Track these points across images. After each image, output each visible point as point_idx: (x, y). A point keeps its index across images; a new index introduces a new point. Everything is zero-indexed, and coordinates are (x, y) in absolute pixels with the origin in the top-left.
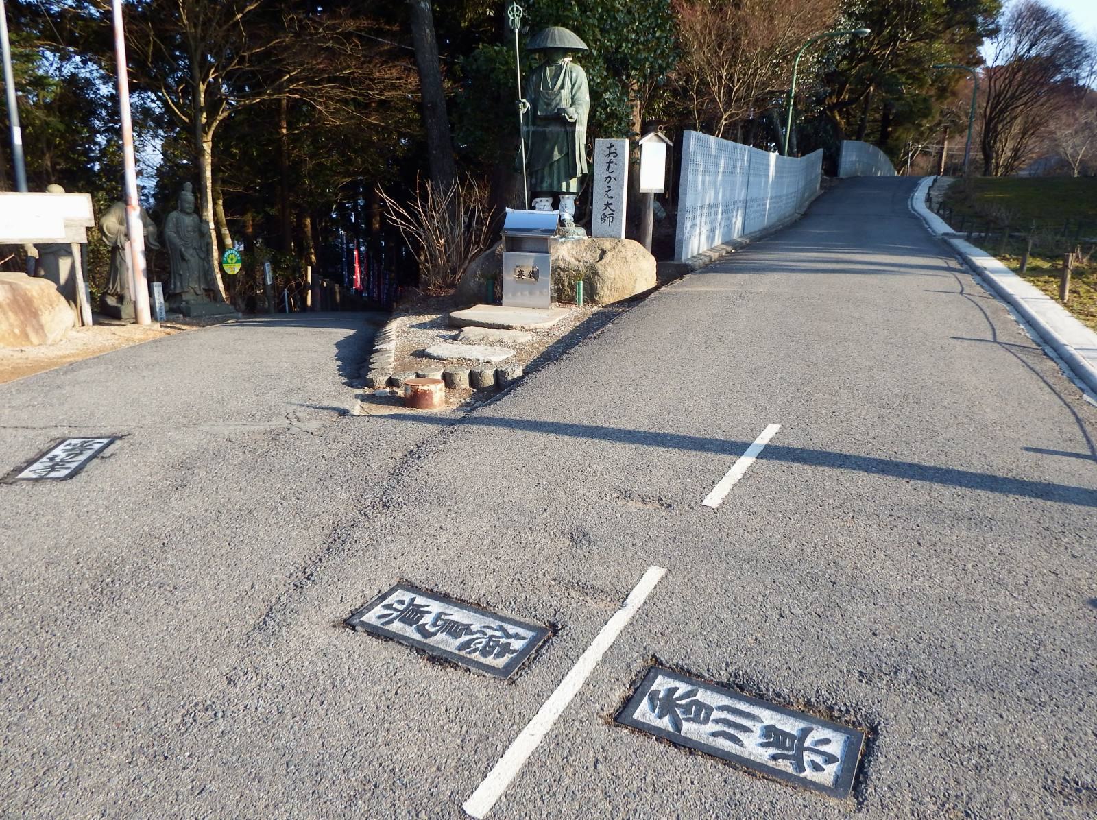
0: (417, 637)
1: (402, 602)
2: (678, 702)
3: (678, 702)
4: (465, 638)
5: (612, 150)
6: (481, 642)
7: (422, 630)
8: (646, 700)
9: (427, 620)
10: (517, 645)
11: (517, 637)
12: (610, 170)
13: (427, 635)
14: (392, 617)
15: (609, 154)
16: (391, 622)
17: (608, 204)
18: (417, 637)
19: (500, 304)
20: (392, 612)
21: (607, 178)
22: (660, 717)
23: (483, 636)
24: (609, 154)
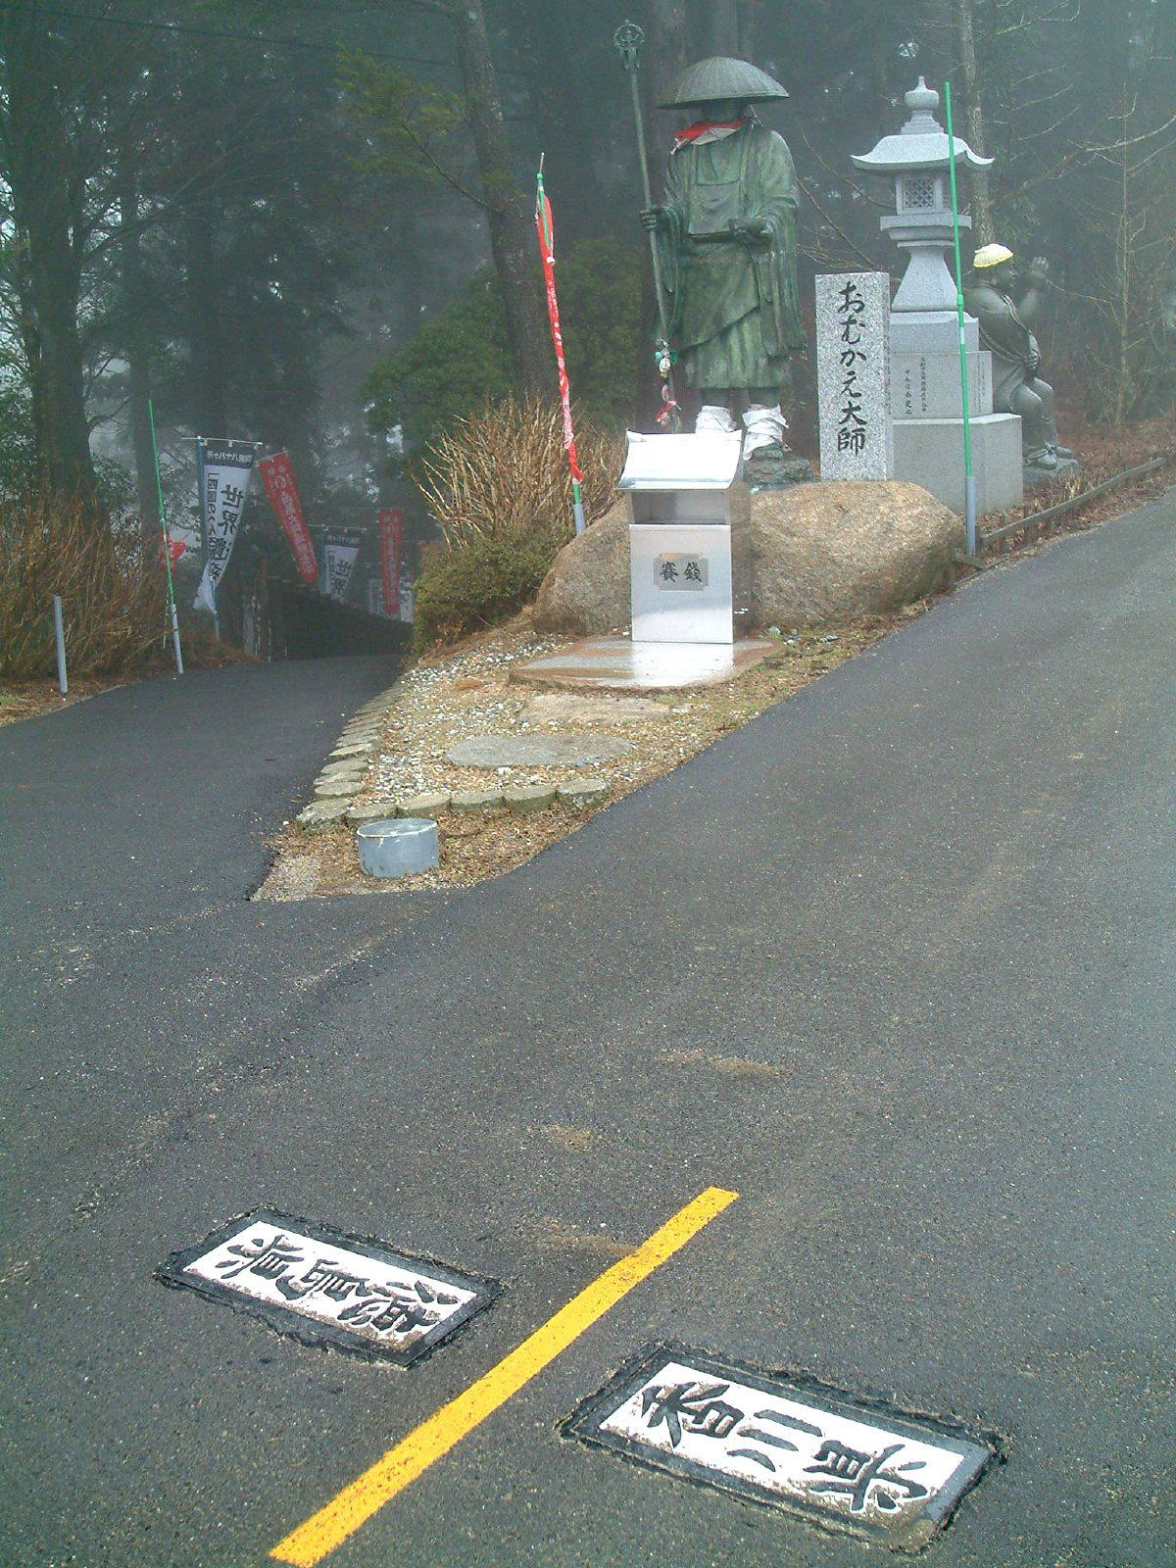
0: (279, 1298)
1: (258, 1242)
2: (685, 1405)
3: (685, 1405)
4: (352, 1300)
5: (853, 295)
6: (378, 1308)
7: (284, 1285)
8: (638, 1397)
9: (296, 1271)
10: (446, 1312)
11: (443, 1300)
12: (852, 337)
13: (292, 1293)
14: (238, 1266)
15: (846, 306)
16: (235, 1273)
17: (849, 411)
18: (279, 1298)
19: (769, 365)
20: (353, 1284)
21: (844, 354)
22: (654, 1422)
23: (382, 1297)
24: (846, 306)
